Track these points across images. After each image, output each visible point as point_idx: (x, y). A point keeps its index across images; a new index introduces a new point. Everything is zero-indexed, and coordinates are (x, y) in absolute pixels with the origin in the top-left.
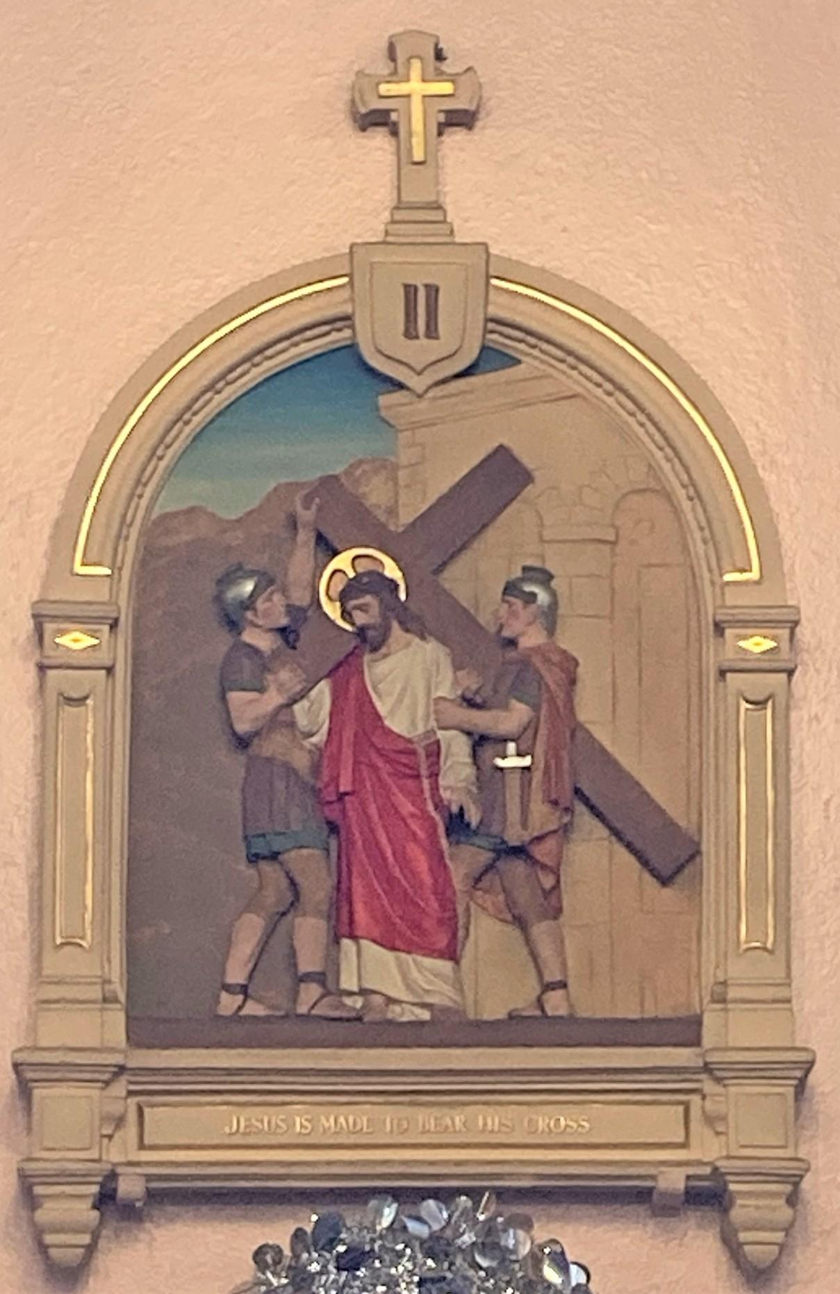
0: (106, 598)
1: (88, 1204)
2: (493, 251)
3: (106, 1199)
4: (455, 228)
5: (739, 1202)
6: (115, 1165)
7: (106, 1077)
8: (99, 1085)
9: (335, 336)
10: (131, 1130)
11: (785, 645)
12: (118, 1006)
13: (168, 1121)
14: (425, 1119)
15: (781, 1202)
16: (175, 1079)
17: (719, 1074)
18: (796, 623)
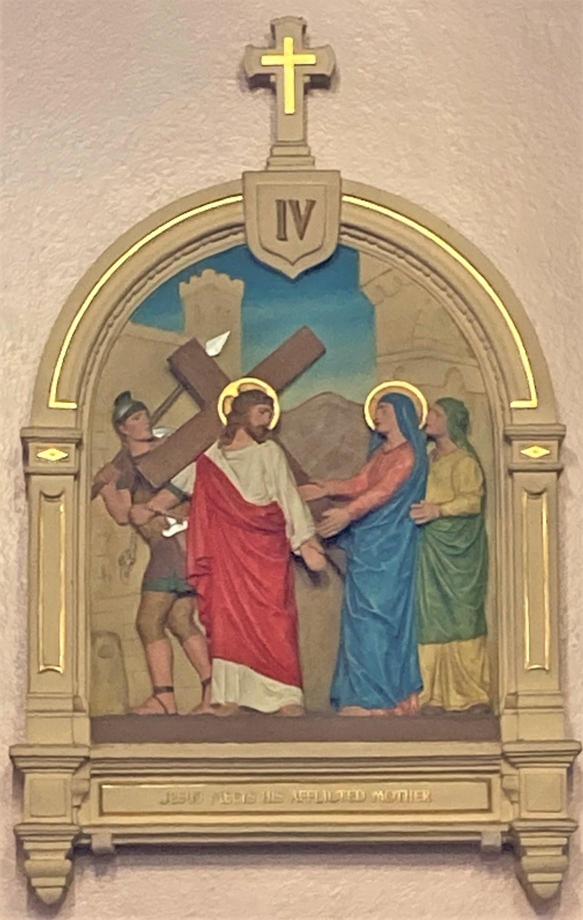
1: (61, 856)
5: (530, 853)
7: (76, 765)
11: (555, 456)
12: (83, 714)
15: (559, 852)
16: (482, 762)
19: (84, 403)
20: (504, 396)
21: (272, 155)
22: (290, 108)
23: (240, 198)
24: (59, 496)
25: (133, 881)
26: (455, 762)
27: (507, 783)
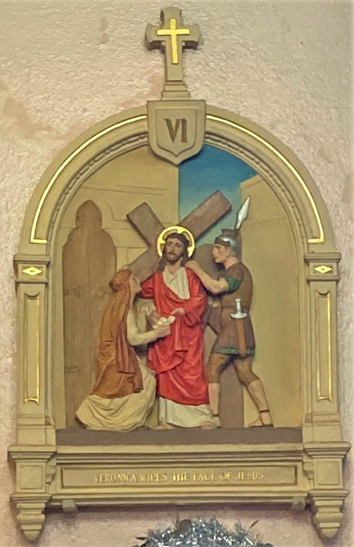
0: (44, 253)
5: (320, 510)
8: (46, 461)
9: (141, 141)
10: (58, 480)
13: (72, 476)
14: (156, 475)
17: (310, 453)
18: (339, 260)
25: (88, 529)
27: (307, 468)
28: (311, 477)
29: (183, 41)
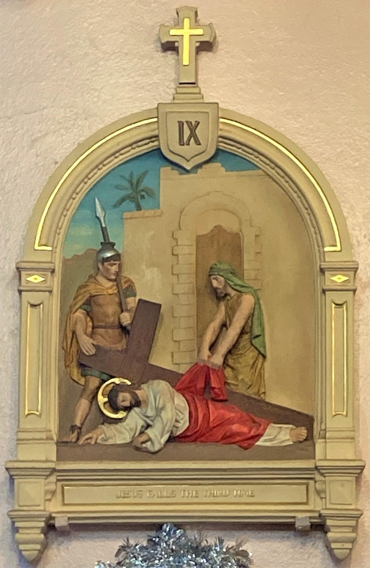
1: (39, 531)
2: (220, 106)
3: (50, 527)
4: (204, 96)
6: (51, 513)
8: (45, 477)
9: (151, 144)
10: (59, 496)
11: (352, 281)
12: (52, 441)
17: (322, 471)
19: (56, 247)
20: (320, 244)
21: (177, 93)
22: (186, 61)
23: (156, 119)
24: (39, 305)
26: (198, 473)
27: (318, 486)
28: (323, 496)
29: (197, 42)
